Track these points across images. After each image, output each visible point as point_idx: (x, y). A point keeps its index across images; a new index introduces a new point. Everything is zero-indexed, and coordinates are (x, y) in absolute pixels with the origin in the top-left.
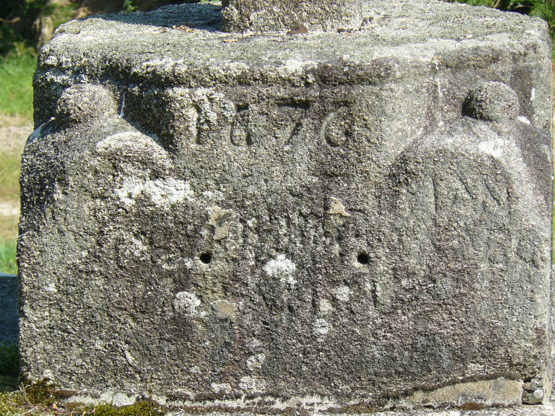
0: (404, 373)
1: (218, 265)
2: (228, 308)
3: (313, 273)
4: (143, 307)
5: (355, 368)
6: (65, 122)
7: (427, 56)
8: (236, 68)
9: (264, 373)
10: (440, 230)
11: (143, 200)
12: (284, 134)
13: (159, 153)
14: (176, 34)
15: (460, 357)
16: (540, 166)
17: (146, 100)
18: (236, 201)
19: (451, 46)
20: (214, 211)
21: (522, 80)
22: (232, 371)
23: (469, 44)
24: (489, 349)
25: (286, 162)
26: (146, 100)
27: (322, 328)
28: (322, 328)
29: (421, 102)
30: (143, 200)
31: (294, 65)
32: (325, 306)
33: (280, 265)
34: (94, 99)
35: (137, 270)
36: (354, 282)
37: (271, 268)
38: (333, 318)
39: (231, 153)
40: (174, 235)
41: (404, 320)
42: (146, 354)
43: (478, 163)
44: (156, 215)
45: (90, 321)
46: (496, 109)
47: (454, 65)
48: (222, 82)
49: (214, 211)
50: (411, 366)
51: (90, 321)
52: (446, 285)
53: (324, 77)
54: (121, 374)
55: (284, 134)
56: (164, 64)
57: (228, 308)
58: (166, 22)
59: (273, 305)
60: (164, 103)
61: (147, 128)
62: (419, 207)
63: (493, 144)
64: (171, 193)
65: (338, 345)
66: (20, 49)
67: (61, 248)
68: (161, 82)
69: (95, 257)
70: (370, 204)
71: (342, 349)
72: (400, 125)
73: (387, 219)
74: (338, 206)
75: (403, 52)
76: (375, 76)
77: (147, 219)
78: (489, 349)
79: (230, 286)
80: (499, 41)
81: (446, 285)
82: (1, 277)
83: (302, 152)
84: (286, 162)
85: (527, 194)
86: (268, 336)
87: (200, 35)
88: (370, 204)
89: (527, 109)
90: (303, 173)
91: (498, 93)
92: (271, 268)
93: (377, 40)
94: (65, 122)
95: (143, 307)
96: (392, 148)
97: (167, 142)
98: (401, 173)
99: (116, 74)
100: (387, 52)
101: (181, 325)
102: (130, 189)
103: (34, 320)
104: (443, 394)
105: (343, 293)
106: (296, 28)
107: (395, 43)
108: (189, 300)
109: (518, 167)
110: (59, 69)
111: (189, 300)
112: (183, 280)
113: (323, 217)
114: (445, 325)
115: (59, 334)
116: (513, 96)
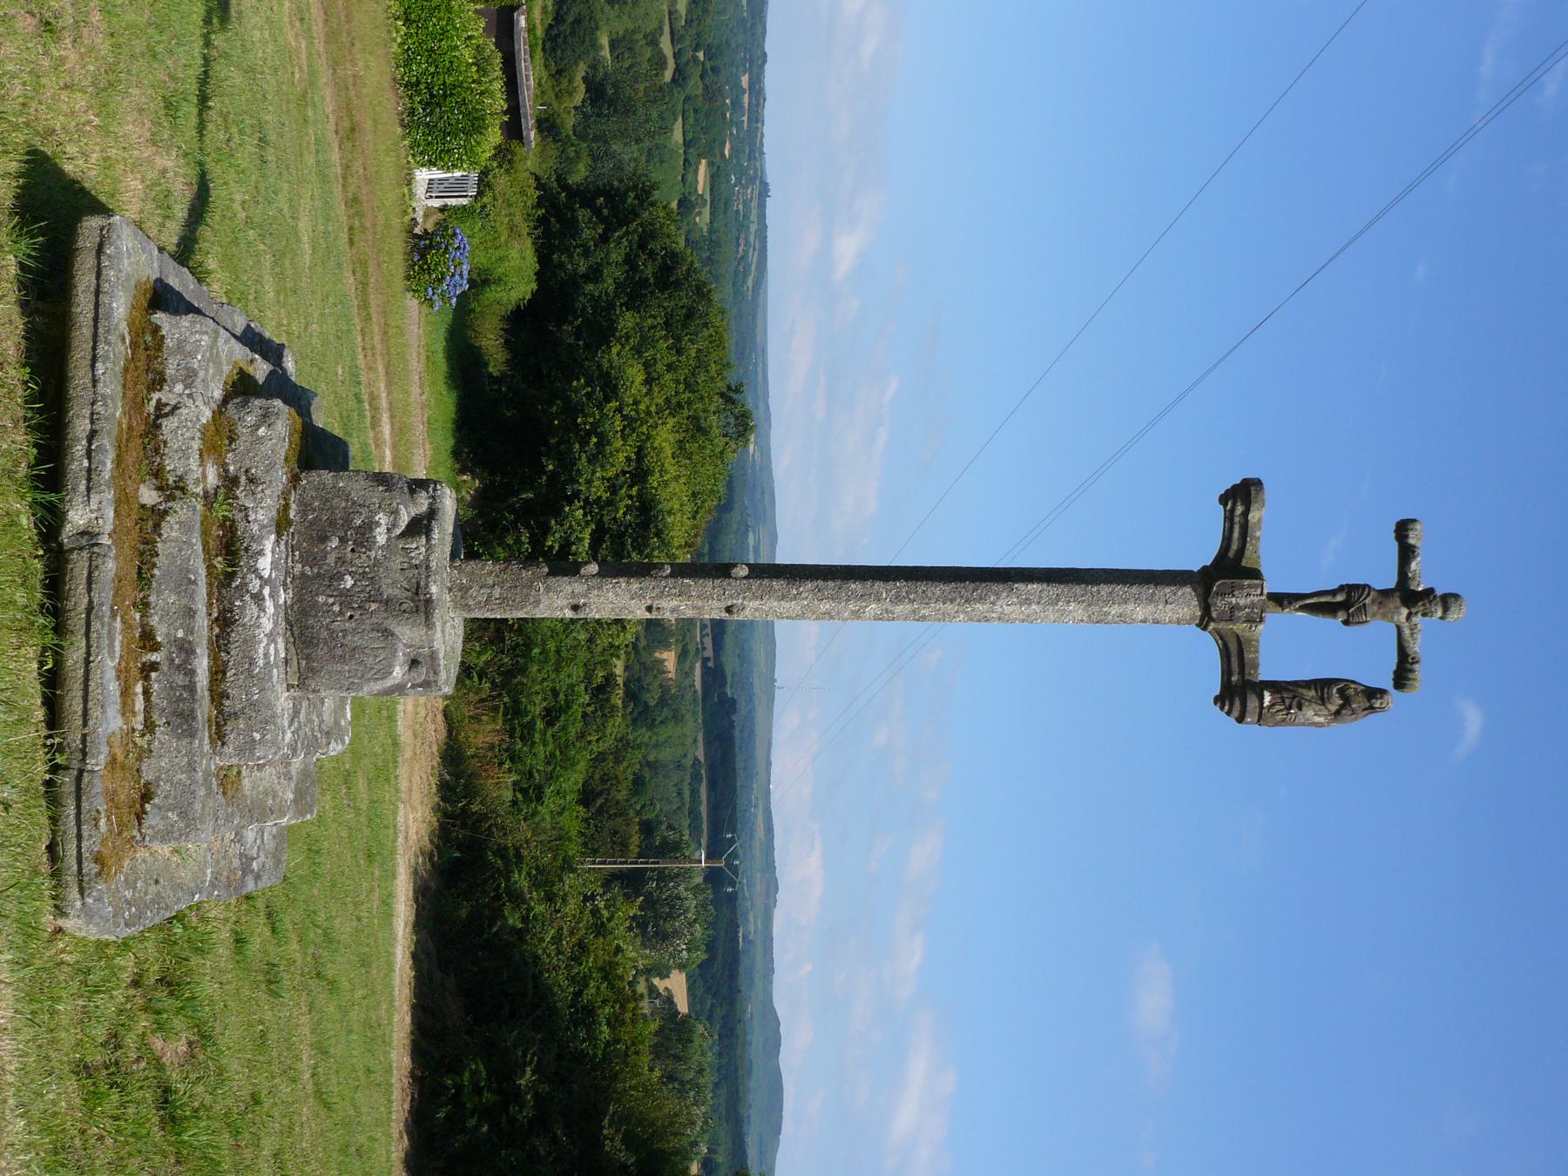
0: (301, 634)
1: (349, 555)
2: (331, 559)
3: (345, 596)
4: (332, 523)
5: (304, 613)
6: (412, 492)
7: (436, 645)
8: (433, 564)
9: (303, 574)
10: (362, 649)
11: (378, 524)
12: (405, 584)
13: (398, 531)
14: (449, 539)
15: (308, 658)
16: (389, 692)
17: (420, 526)
18: (377, 563)
19: (441, 655)
20: (373, 554)
21: (426, 684)
22: (304, 561)
23: (442, 662)
24: (311, 670)
25: (393, 585)
26: (420, 526)
27: (321, 599)
28: (321, 599)
29: (416, 642)
30: (378, 524)
31: (434, 589)
32: (331, 600)
33: (349, 582)
34: (422, 504)
35: (348, 522)
36: (341, 613)
37: (348, 577)
38: (325, 604)
39: (397, 562)
40: (364, 536)
41: (324, 634)
42: (312, 523)
43: (391, 666)
44: (371, 530)
45: (327, 500)
46: (414, 674)
47: (433, 656)
48: (427, 559)
49: (373, 554)
50: (176, 851)
51: (327, 500)
52: (339, 652)
53: (429, 602)
54: (303, 513)
55: (405, 584)
56: (436, 535)
57: (331, 559)
58: (454, 535)
59: (331, 578)
60: (419, 534)
61: (408, 526)
62: (374, 641)
63: (398, 672)
64: (381, 537)
65: (315, 605)
66: (458, 466)
67: (357, 488)
68: (428, 533)
69: (354, 503)
70: (374, 620)
71: (312, 607)
72: (407, 633)
73: (368, 627)
74: (374, 606)
75: (439, 635)
76: (429, 623)
77: (370, 525)
78: (311, 670)
79: (340, 560)
80: (443, 675)
81: (339, 652)
82: (413, 1162)
83: (397, 592)
84: (393, 585)
85: (378, 686)
86: (319, 575)
87: (448, 550)
88: (374, 620)
89: (413, 686)
90: (388, 592)
91: (422, 674)
92: (348, 577)
93: (444, 623)
94: (412, 492)
95: (332, 523)
96: (398, 630)
97: (403, 535)
98: (387, 634)
99: (432, 513)
100: (439, 628)
101: (324, 539)
102: (382, 518)
103: (327, 476)
104: (293, 650)
105: (336, 608)
106: (450, 590)
107: (443, 632)
108: (335, 543)
109: (389, 683)
110: (435, 490)
111: (335, 543)
112: (343, 540)
113: (369, 600)
114: (321, 652)
115: (321, 487)
116: (419, 681)
